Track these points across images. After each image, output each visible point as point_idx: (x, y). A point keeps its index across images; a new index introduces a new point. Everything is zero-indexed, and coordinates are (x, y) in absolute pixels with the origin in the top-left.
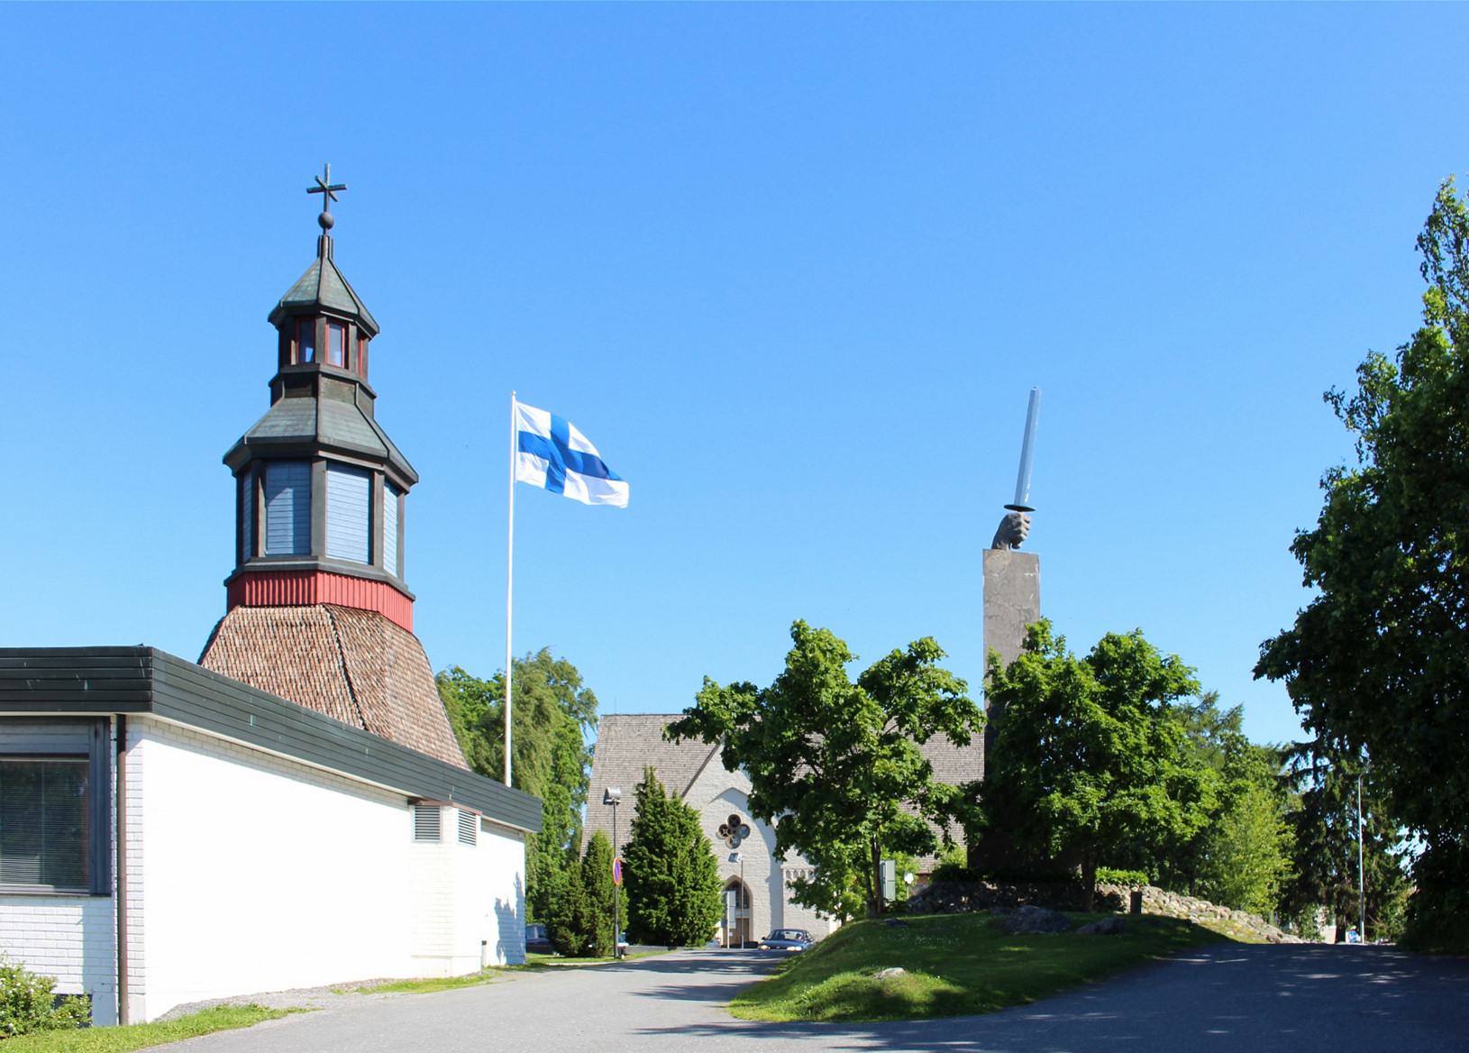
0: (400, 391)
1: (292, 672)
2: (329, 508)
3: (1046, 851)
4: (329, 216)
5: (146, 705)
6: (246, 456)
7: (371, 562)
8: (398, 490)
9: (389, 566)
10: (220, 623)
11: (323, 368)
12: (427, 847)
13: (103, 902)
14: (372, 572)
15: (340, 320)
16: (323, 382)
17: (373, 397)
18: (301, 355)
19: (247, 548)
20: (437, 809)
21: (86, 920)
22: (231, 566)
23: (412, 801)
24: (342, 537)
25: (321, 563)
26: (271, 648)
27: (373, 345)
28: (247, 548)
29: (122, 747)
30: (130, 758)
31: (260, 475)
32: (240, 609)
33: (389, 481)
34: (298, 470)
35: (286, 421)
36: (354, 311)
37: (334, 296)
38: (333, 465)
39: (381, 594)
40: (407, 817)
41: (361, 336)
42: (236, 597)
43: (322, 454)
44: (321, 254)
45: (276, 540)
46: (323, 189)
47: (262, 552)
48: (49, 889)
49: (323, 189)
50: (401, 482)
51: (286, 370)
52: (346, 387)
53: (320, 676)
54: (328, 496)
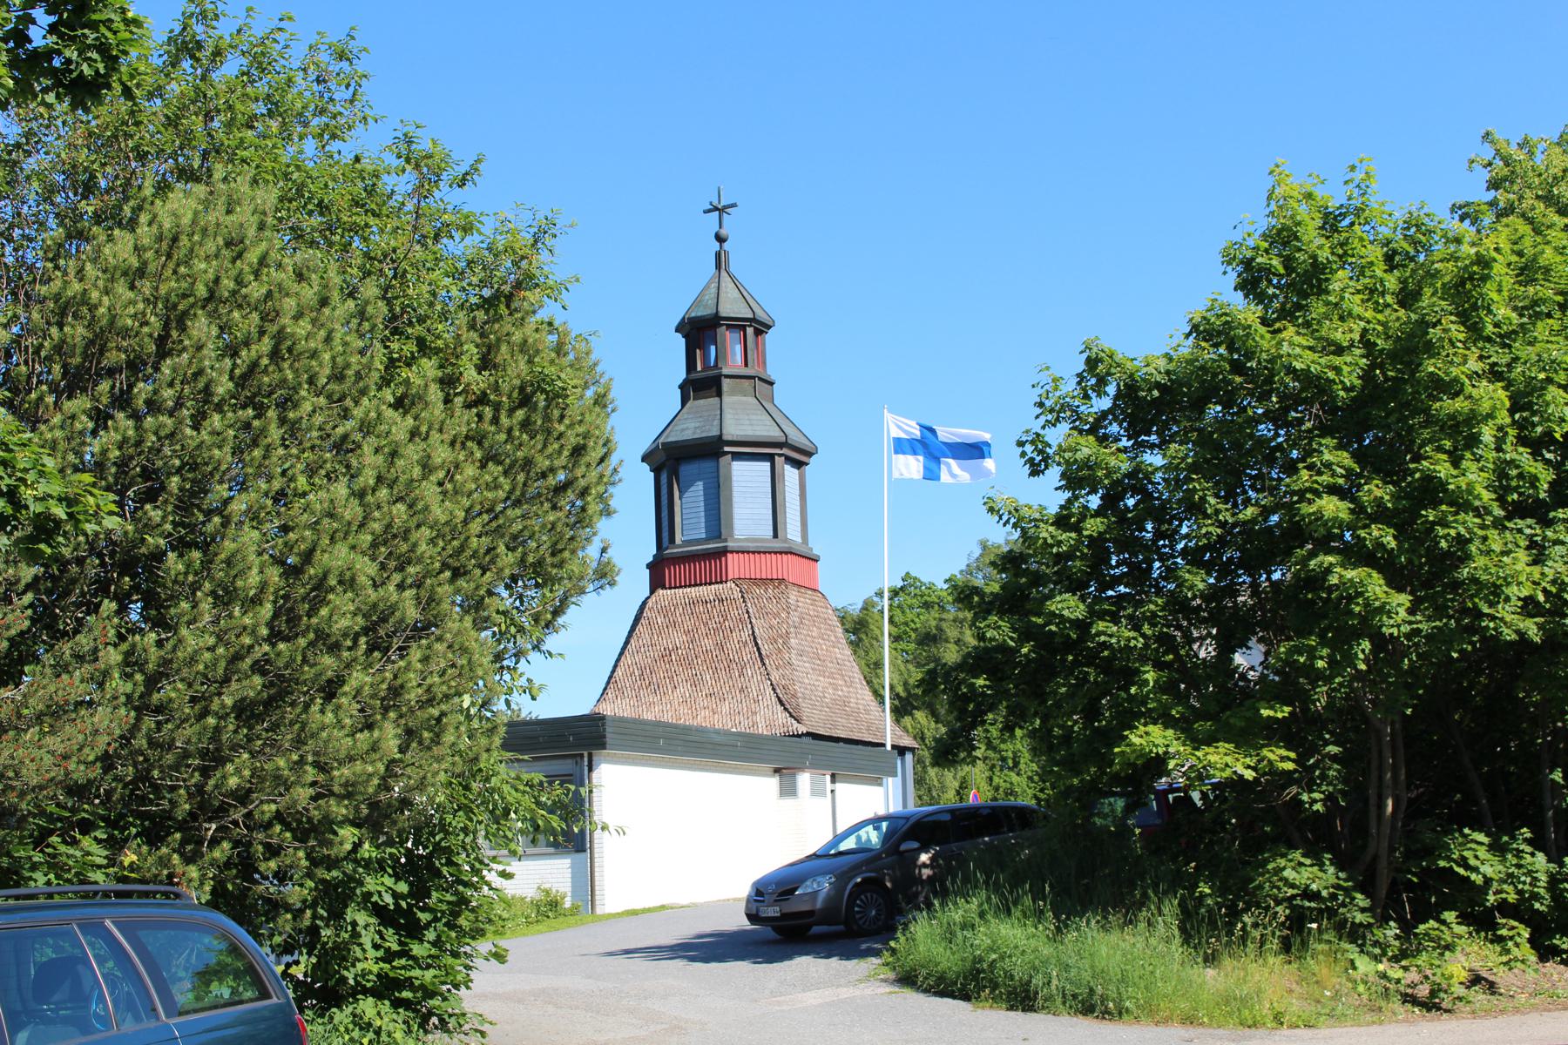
0: (801, 378)
1: (708, 643)
2: (735, 494)
3: (1295, 771)
4: (723, 232)
5: (603, 746)
6: (661, 457)
7: (775, 536)
8: (798, 464)
9: (793, 532)
10: (644, 603)
11: (725, 371)
12: (788, 802)
13: (581, 855)
14: (777, 545)
15: (738, 325)
16: (726, 383)
17: (772, 384)
18: (705, 357)
19: (665, 535)
20: (794, 775)
21: (572, 867)
22: (652, 550)
23: (777, 771)
24: (748, 514)
25: (731, 544)
26: (688, 624)
27: (770, 337)
28: (665, 535)
29: (590, 770)
30: (595, 775)
31: (674, 473)
32: (661, 592)
33: (789, 460)
34: (707, 465)
35: (692, 429)
36: (750, 316)
37: (732, 307)
38: (737, 456)
39: (790, 556)
40: (773, 782)
41: (758, 333)
42: (657, 583)
43: (727, 449)
44: (718, 266)
45: (690, 527)
46: (716, 209)
47: (678, 539)
48: (552, 850)
49: (716, 209)
50: (800, 456)
51: (693, 376)
52: (746, 383)
53: (732, 645)
54: (734, 484)
